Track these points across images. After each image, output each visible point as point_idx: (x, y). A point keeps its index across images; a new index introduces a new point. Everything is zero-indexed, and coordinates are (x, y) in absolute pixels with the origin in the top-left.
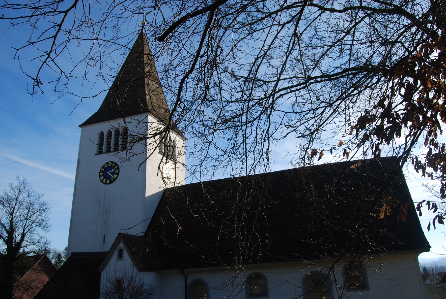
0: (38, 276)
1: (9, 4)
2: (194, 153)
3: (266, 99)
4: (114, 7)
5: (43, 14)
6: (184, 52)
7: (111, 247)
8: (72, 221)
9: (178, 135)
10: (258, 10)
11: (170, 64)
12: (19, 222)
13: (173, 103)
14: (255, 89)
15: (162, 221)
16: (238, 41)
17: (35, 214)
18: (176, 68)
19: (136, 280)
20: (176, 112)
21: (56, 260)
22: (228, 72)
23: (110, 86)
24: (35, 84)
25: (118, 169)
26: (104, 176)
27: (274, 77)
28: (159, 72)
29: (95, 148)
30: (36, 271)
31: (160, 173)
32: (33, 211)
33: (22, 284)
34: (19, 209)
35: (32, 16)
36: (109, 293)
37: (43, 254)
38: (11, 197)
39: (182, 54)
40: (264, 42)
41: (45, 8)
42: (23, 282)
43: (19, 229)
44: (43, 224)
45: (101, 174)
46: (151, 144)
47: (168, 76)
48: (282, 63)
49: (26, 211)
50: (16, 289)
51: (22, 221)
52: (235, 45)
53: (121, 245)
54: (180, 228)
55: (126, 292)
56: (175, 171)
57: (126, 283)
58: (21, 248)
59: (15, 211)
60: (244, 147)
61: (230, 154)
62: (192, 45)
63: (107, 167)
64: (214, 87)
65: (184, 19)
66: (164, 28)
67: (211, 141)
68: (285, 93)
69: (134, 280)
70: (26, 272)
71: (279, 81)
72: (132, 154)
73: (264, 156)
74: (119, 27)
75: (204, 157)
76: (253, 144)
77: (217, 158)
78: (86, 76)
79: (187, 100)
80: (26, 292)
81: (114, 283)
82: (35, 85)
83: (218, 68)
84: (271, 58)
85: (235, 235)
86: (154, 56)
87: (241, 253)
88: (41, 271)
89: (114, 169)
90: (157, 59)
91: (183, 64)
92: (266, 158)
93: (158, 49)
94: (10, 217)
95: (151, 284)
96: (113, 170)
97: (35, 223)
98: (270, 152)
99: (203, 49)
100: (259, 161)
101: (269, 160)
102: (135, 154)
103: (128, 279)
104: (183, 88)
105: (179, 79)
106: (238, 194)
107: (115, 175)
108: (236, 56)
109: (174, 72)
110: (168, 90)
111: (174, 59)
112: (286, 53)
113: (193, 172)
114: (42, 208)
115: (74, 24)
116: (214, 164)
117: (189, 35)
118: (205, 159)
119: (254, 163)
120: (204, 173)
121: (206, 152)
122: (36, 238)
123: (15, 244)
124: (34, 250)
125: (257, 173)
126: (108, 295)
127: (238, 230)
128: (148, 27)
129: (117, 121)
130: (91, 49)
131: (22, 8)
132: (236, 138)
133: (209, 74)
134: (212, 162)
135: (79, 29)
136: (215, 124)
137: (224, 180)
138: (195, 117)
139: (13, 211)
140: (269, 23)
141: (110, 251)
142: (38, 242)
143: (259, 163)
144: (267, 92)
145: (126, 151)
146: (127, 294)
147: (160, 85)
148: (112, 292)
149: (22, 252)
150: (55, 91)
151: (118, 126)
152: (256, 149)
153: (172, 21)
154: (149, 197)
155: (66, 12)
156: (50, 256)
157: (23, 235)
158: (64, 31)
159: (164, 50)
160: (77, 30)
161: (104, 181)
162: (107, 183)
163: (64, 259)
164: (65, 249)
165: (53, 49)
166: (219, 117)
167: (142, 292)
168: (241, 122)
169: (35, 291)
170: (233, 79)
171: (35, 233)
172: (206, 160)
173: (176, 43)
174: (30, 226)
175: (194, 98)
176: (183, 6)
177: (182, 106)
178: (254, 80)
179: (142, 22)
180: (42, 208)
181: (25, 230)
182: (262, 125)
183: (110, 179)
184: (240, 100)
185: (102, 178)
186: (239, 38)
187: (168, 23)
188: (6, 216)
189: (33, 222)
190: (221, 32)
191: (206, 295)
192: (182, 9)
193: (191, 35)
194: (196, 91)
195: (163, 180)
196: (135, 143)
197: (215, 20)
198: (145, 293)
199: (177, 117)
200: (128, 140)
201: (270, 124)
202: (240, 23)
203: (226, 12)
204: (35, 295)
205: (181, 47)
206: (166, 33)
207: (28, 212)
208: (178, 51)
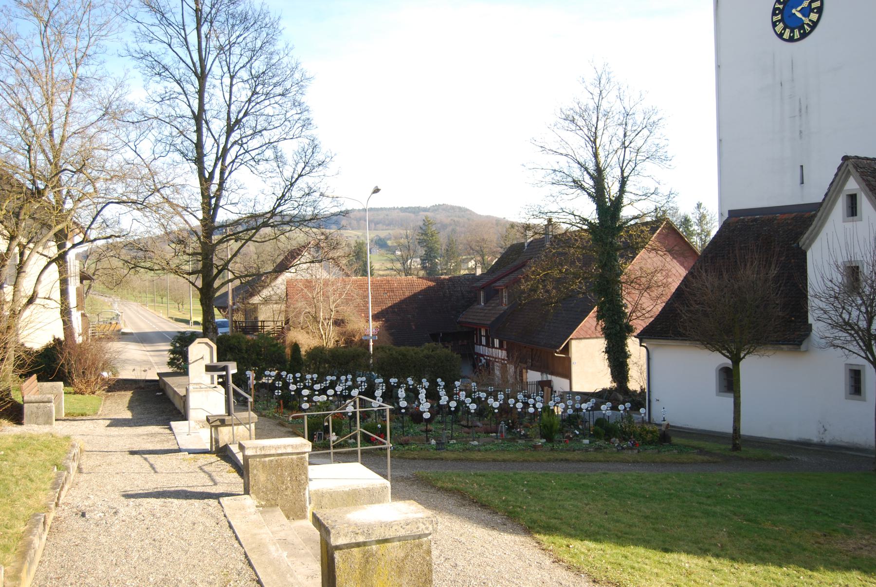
12: (610, 156)
26: (784, 24)
53: (852, 185)
94: (592, 147)
126: (836, 298)
139: (595, 133)
141: (824, 200)
157: (623, 182)
162: (795, 38)
185: (780, 26)
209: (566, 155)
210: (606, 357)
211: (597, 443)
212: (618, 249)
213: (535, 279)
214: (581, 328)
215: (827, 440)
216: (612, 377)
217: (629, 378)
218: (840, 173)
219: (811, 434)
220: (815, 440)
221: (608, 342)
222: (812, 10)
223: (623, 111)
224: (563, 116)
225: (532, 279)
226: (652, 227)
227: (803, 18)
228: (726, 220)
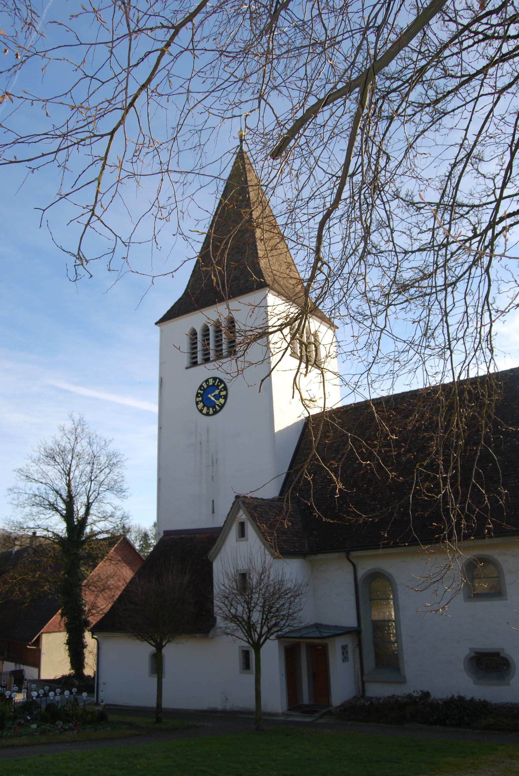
0: (115, 569)
1: (22, 138)
2: (355, 353)
3: (478, 239)
4: (189, 111)
5: (75, 144)
6: (318, 173)
7: (225, 519)
8: (159, 480)
9: (323, 322)
10: (446, 75)
11: (297, 197)
12: (80, 486)
13: (309, 266)
14: (456, 223)
15: (307, 476)
16: (416, 137)
17: (103, 472)
18: (308, 203)
19: (271, 573)
20: (314, 283)
21: (142, 542)
22: (401, 198)
23: (199, 250)
24: (77, 264)
25: (225, 388)
26: (203, 403)
27: (488, 196)
28: (279, 215)
29: (185, 359)
30: (112, 562)
31: (296, 391)
32: (99, 467)
33: (94, 582)
34: (77, 466)
35: (59, 150)
36: (229, 594)
37: (121, 535)
38: (64, 447)
39: (316, 178)
40: (465, 132)
41: (77, 133)
42: (95, 579)
43: (81, 497)
44: (116, 487)
45: (198, 399)
46: (276, 343)
47: (295, 219)
48: (502, 166)
49: (89, 468)
50: (85, 591)
51: (84, 485)
52: (411, 146)
53: (242, 516)
54: (340, 486)
55: (256, 593)
56: (323, 387)
57: (254, 579)
58: (86, 526)
59: (73, 469)
60: (445, 332)
61: (420, 347)
62: (332, 158)
63: (207, 388)
64: (377, 229)
65: (314, 111)
66: (280, 135)
67: (382, 328)
68: (512, 223)
69: (267, 573)
70: (98, 564)
71: (500, 202)
72: (247, 365)
73: (484, 344)
74: (202, 146)
75: (373, 357)
76: (461, 325)
77: (396, 357)
78: (155, 238)
79: (332, 258)
80: (101, 595)
81: (235, 579)
82: (78, 265)
83: (382, 193)
84: (480, 160)
85: (441, 493)
86: (267, 186)
87: (454, 524)
88: (119, 561)
89: (218, 389)
90: (274, 192)
91: (319, 195)
92: (488, 348)
93: (274, 172)
94: (66, 479)
95: (296, 579)
96: (217, 392)
97: (104, 486)
98: (494, 337)
99: (353, 160)
100: (475, 354)
101: (493, 351)
102: (251, 364)
103: (257, 571)
104: (325, 238)
105: (315, 224)
106: (441, 418)
107: (221, 399)
108: (415, 165)
109: (305, 211)
110: (298, 244)
111: (302, 189)
112: (511, 146)
113: (354, 386)
114: (111, 462)
115: (126, 151)
116: (391, 369)
117: (325, 140)
118: (374, 360)
119: (466, 359)
120: (376, 385)
121: (375, 347)
122: (107, 510)
123: (78, 520)
124: (106, 529)
125: (472, 375)
126: (227, 598)
127: (445, 485)
128: (251, 137)
129: (216, 309)
130: (159, 191)
131: (41, 140)
132: (428, 317)
133: (368, 206)
134: (389, 365)
135: (135, 159)
136: (387, 295)
137: (410, 394)
138: (349, 287)
139: (70, 469)
140: (469, 94)
141: (224, 525)
142: (111, 516)
143: (474, 359)
144: (477, 226)
145: (236, 360)
146: (257, 596)
147: (283, 238)
148: (233, 594)
149: (90, 533)
150: (109, 270)
151: (218, 317)
152: (467, 334)
153: (291, 119)
154: (281, 432)
155: (112, 134)
156: (131, 537)
157: (88, 507)
158: (111, 166)
159: (284, 175)
160: (132, 162)
161: (205, 411)
162: (210, 413)
163: (153, 541)
164: (153, 524)
165: (98, 199)
166: (394, 281)
167: (282, 593)
168: (436, 287)
169: (114, 592)
170: (412, 210)
171: (105, 502)
172: (377, 363)
173: (303, 159)
174: (97, 492)
175: (345, 254)
176: (308, 88)
177: (325, 269)
178: (452, 206)
179: (239, 132)
180: (111, 462)
181: (91, 498)
182: (474, 287)
183: (214, 407)
184: (429, 246)
185: (201, 405)
186: (416, 131)
187: (285, 124)
188: (60, 478)
189: (101, 484)
190: (383, 125)
191: (391, 597)
192: (308, 94)
193: (328, 140)
194: (347, 240)
195: (304, 405)
196: (249, 344)
197: (371, 103)
198: (287, 594)
199: (318, 292)
200: (237, 341)
201: (489, 285)
202: (413, 104)
203: (386, 88)
204: (115, 599)
205: (312, 164)
206: (285, 141)
207: (92, 470)
208: (308, 172)
209: (46, 484)
210: (67, 647)
211: (43, 727)
212: (81, 559)
213: (13, 582)
214: (51, 623)
215: (228, 708)
216: (71, 665)
217: (85, 665)
218: (234, 507)
219: (217, 703)
220: (220, 707)
221: (69, 635)
222: (221, 397)
223: (91, 454)
224: (46, 454)
225: (10, 582)
226: (109, 542)
227: (216, 401)
228: (162, 538)
